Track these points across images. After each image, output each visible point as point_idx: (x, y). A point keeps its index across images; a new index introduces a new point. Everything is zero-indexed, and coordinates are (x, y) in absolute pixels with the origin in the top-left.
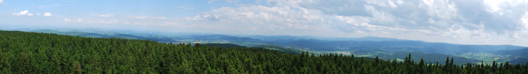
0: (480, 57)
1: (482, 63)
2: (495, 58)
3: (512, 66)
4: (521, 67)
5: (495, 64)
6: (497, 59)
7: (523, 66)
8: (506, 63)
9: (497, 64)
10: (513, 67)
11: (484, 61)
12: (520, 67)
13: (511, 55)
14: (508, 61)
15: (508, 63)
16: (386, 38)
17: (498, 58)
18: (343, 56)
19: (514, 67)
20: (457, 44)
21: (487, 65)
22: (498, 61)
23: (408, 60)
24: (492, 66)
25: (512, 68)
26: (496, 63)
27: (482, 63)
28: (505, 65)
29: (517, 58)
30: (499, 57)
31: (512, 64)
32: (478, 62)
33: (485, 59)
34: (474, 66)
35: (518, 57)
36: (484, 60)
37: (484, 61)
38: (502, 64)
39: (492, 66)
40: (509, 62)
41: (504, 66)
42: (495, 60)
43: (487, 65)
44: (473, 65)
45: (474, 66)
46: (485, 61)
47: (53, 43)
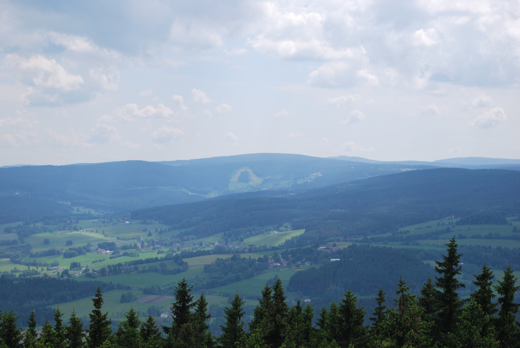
0: (77, 259)
1: (98, 303)
2: (191, 262)
3: (308, 318)
4: (367, 323)
5: (192, 310)
6: (207, 269)
7: (379, 312)
8: (266, 294)
9: (202, 304)
10: (314, 324)
11: (111, 287)
12: (358, 323)
13: (296, 227)
14: (277, 286)
15: (280, 296)
16: (425, 162)
17: (211, 259)
18: (46, 274)
19: (322, 323)
20: (473, 169)
21: (132, 321)
22: (212, 285)
23: (273, 293)
24: (170, 325)
25: (307, 333)
26: (196, 298)
27: (98, 303)
28: (259, 314)
29: (339, 253)
30: (219, 251)
31: (307, 300)
32: (63, 300)
33: (116, 270)
34: (39, 331)
35: (343, 245)
36: (106, 280)
37: (111, 287)
38: (237, 303)
39: (170, 325)
40: (284, 286)
41: (252, 317)
42: (188, 276)
43: (132, 321)
44: (32, 325)
45: (39, 331)
46: (120, 287)
47: (455, 281)
